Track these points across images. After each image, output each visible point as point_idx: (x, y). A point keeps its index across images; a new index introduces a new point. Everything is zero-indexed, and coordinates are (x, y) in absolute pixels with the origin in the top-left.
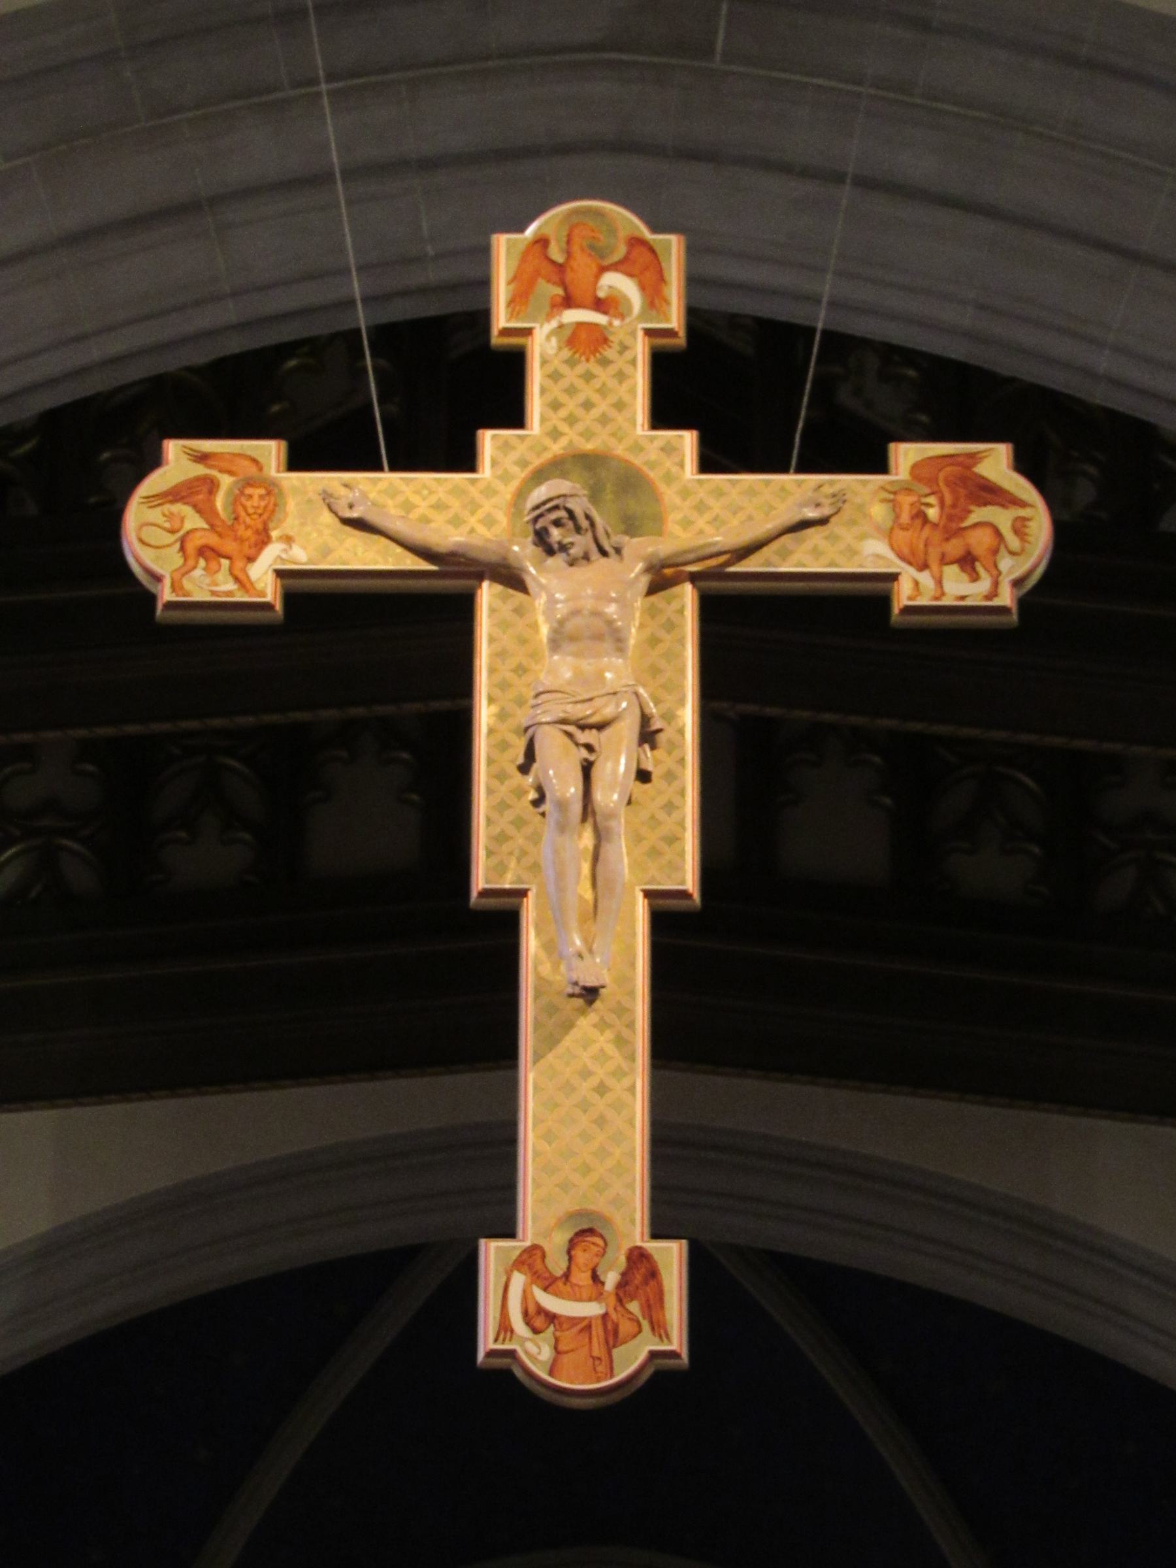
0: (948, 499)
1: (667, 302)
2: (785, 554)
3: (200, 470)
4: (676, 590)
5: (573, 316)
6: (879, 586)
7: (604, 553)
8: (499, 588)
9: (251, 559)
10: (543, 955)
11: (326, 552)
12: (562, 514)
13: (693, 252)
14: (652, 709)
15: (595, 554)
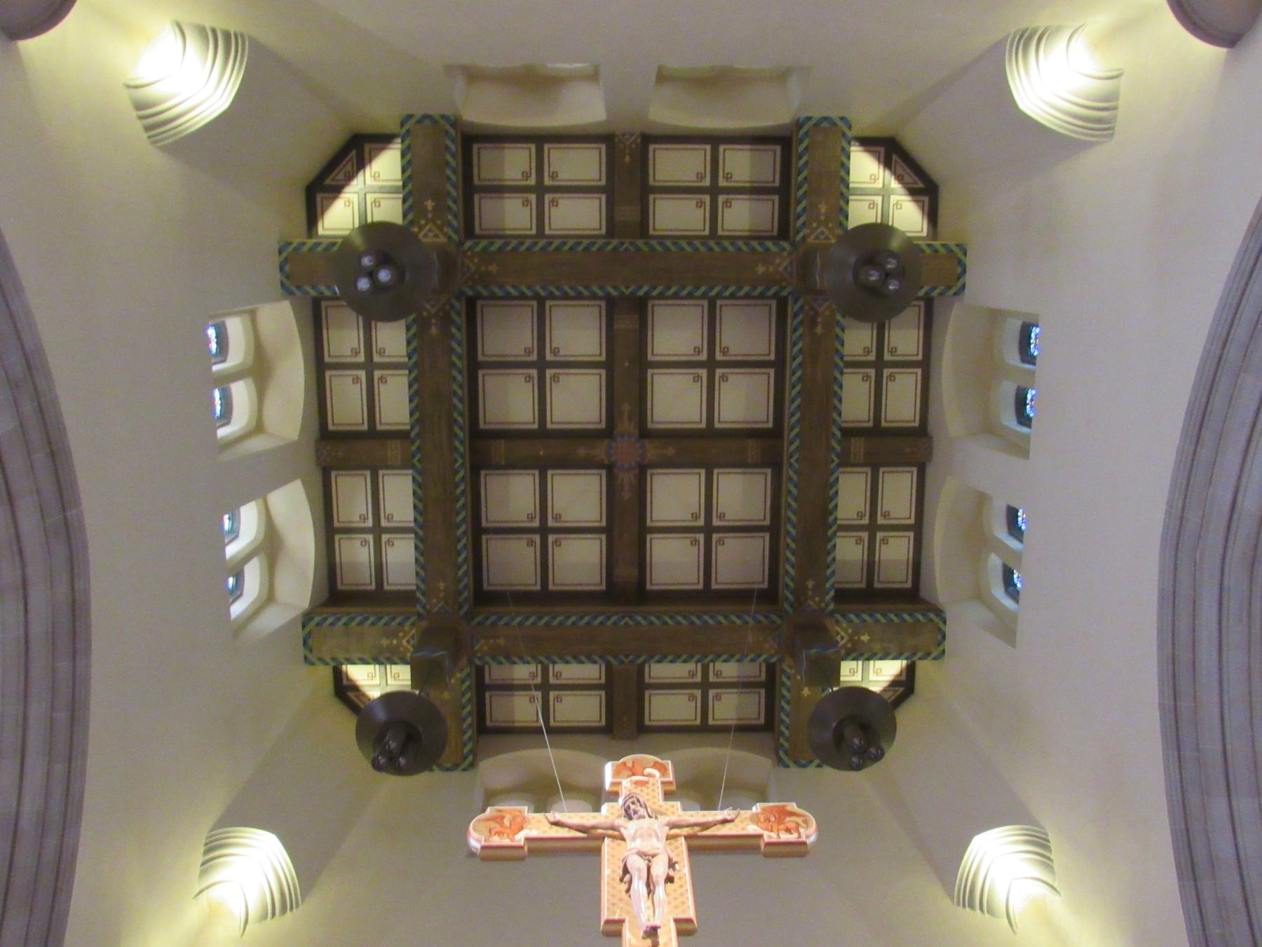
0: (777, 816)
1: (669, 775)
2: (718, 830)
3: (499, 813)
4: (679, 839)
5: (635, 778)
6: (752, 841)
7: (650, 817)
8: (610, 839)
9: (516, 834)
10: (632, 937)
11: (544, 832)
12: (634, 799)
13: (672, 762)
14: (672, 855)
15: (647, 817)
